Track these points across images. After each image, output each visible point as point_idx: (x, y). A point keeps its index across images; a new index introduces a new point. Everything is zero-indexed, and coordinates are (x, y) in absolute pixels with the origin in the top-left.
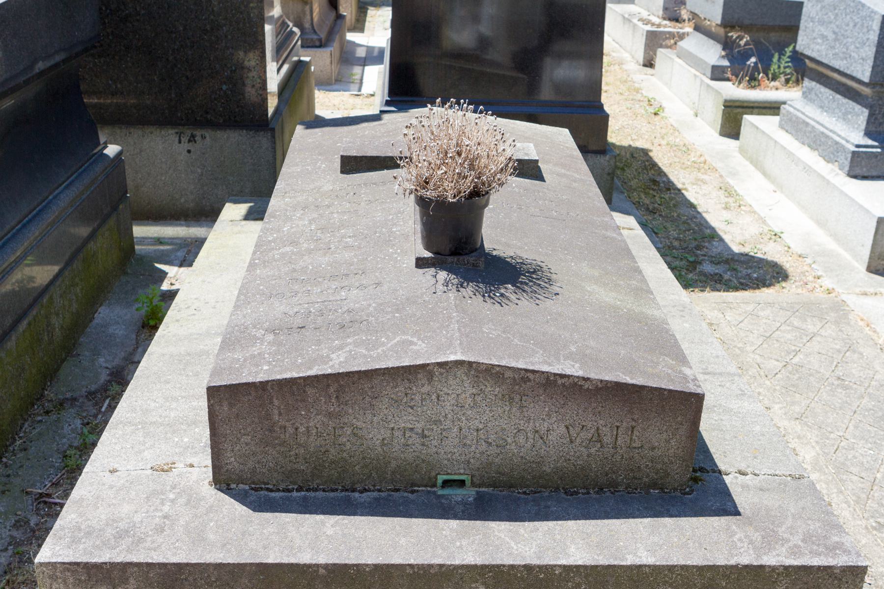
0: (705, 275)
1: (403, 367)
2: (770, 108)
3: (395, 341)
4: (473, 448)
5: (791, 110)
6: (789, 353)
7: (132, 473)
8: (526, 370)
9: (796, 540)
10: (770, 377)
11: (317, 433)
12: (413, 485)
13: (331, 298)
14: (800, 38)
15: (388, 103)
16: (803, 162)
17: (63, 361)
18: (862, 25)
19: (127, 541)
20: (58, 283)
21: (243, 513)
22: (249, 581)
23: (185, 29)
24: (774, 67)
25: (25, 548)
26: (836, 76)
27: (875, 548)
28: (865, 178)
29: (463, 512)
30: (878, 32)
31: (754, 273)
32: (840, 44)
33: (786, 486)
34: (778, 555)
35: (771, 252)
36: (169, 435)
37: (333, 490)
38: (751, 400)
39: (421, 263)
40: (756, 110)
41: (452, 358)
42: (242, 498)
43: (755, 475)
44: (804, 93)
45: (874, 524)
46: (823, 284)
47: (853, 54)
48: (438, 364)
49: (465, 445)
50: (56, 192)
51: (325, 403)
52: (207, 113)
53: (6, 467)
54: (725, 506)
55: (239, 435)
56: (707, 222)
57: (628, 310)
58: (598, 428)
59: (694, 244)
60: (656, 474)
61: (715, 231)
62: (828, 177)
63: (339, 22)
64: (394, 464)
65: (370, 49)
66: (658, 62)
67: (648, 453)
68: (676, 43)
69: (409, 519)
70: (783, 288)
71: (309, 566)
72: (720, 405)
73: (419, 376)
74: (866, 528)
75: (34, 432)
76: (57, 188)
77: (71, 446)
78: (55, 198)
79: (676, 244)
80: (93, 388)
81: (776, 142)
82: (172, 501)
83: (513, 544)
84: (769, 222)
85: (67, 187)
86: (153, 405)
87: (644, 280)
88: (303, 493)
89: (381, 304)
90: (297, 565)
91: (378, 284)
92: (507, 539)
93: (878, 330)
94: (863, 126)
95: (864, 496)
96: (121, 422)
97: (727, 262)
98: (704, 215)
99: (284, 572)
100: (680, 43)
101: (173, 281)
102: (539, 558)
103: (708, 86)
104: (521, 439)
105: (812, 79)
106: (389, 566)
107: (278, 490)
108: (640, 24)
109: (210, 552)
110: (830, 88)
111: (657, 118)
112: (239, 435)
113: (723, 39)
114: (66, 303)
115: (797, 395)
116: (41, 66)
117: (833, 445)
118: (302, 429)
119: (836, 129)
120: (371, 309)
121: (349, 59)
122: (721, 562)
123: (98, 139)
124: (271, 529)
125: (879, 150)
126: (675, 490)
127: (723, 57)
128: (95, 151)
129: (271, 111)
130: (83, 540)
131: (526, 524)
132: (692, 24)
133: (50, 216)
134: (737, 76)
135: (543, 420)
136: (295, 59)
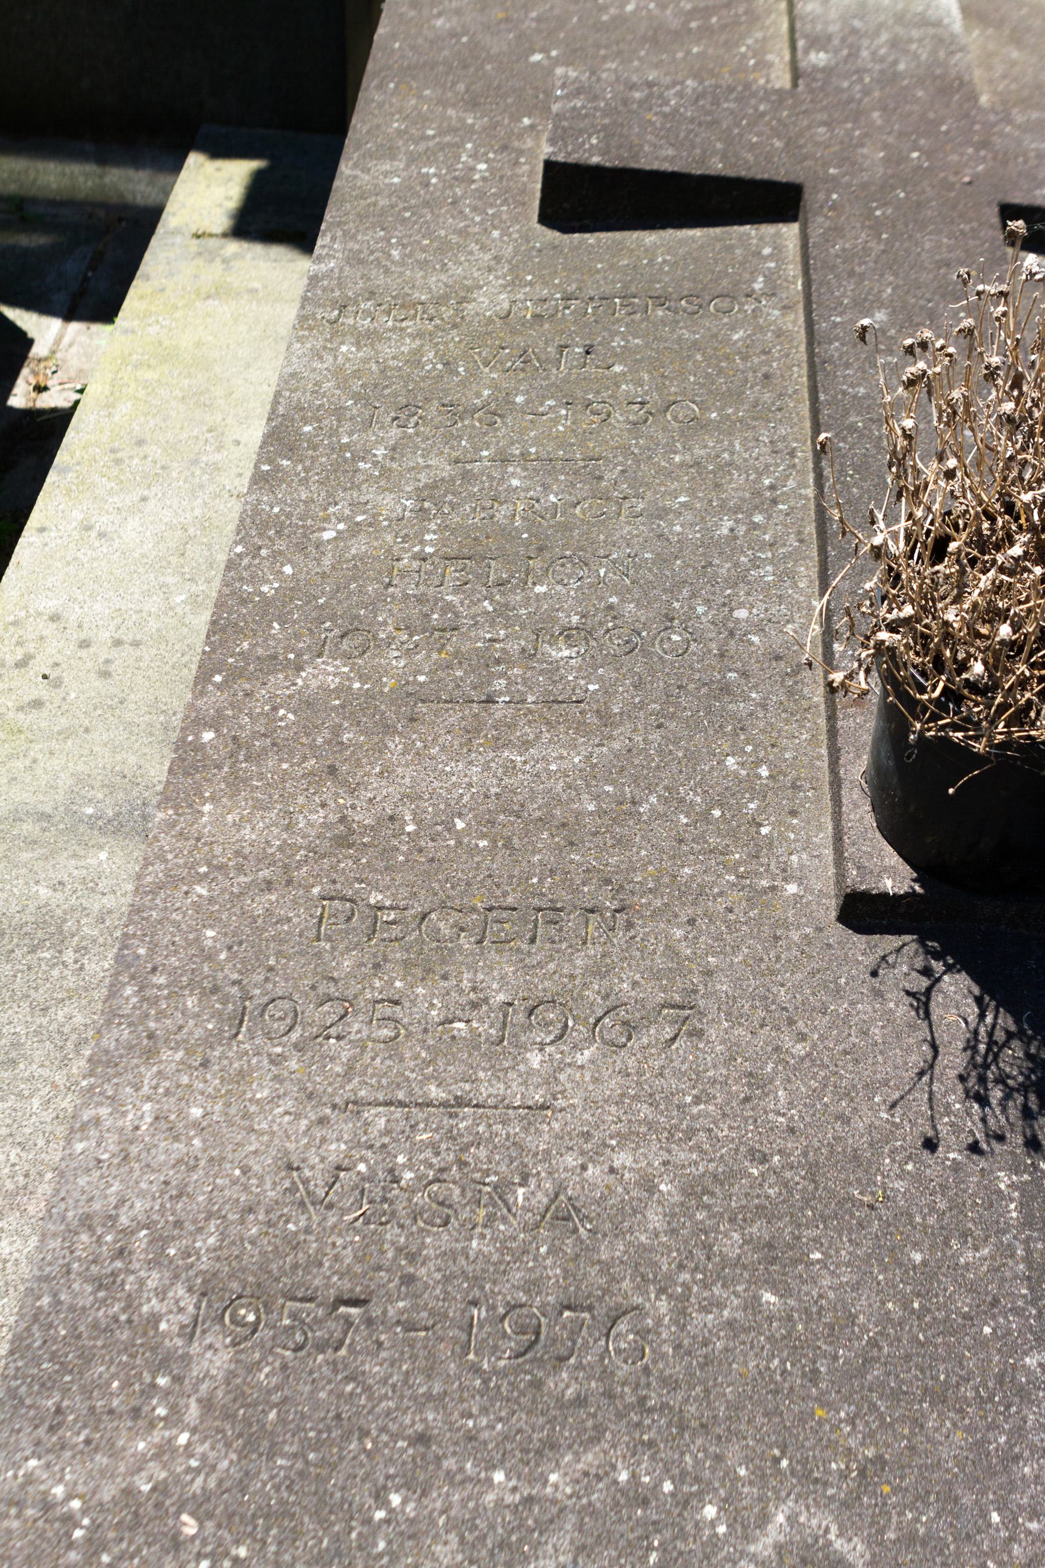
39: (862, 912)
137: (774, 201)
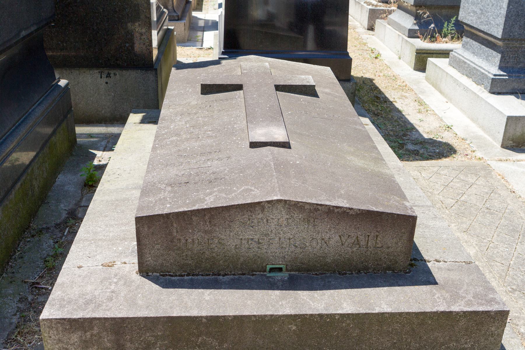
0: (409, 151)
1: (247, 204)
2: (443, 54)
3: (242, 189)
4: (287, 249)
5: (456, 55)
6: (458, 194)
7: (91, 268)
8: (317, 204)
9: (470, 297)
10: (448, 208)
11: (198, 242)
12: (253, 271)
13: (202, 166)
14: (460, 13)
15: (223, 53)
16: (464, 85)
17: (39, 206)
18: (497, 5)
19: (91, 306)
20: (36, 161)
21: (157, 289)
22: (163, 327)
23: (104, 11)
24: (445, 30)
25: (26, 314)
26: (481, 34)
27: (511, 303)
28: (499, 93)
29: (282, 285)
30: (506, 9)
31: (438, 150)
32: (484, 16)
33: (462, 268)
34: (460, 306)
35: (446, 137)
36: (110, 246)
37: (207, 275)
38: (440, 220)
40: (434, 55)
41: (275, 198)
42: (156, 281)
43: (445, 262)
44: (463, 45)
45: (510, 290)
46: (476, 155)
47: (492, 22)
48: (267, 201)
49: (282, 247)
50: (33, 107)
51: (203, 225)
52: (117, 60)
53: (12, 267)
54: (429, 279)
55: (154, 245)
56: (408, 121)
57: (372, 170)
58: (357, 237)
59: (401, 133)
60: (390, 262)
61: (413, 126)
62: (478, 93)
63: (188, 5)
64: (242, 259)
65: (206, 21)
66: (376, 27)
67: (387, 248)
68: (386, 16)
69: (252, 291)
70: (454, 157)
71: (197, 317)
72: (423, 224)
73: (257, 209)
74: (506, 291)
75: (27, 247)
76: (34, 105)
77: (48, 255)
78: (33, 111)
79: (391, 133)
80: (58, 221)
81: (447, 73)
82: (116, 283)
83: (311, 303)
84: (444, 120)
85: (39, 105)
86: (99, 229)
87: (379, 153)
88: (190, 277)
89: (232, 169)
90: (190, 317)
91: (229, 157)
92: (308, 300)
93: (509, 181)
94: (498, 64)
95: (504, 274)
96: (82, 240)
97: (421, 143)
98: (407, 116)
99: (183, 321)
100: (390, 16)
101: (101, 159)
102: (327, 310)
103: (407, 41)
104: (314, 244)
105: (468, 37)
106: (242, 316)
107: (176, 276)
108: (365, 5)
109: (140, 311)
110: (478, 42)
111: (377, 60)
112: (154, 245)
113: (415, 14)
114: (41, 172)
115: (464, 218)
116: (24, 33)
117: (485, 246)
118: (190, 240)
119: (482, 66)
120: (226, 171)
121: (195, 29)
122: (428, 310)
123: (55, 76)
124: (174, 298)
125: (507, 77)
126: (401, 271)
127: (415, 24)
128: (53, 83)
129: (154, 58)
130: (67, 306)
131: (318, 291)
132: (396, 5)
133: (30, 122)
134: (423, 35)
135: (327, 232)
136: (165, 27)
137: (239, 87)
